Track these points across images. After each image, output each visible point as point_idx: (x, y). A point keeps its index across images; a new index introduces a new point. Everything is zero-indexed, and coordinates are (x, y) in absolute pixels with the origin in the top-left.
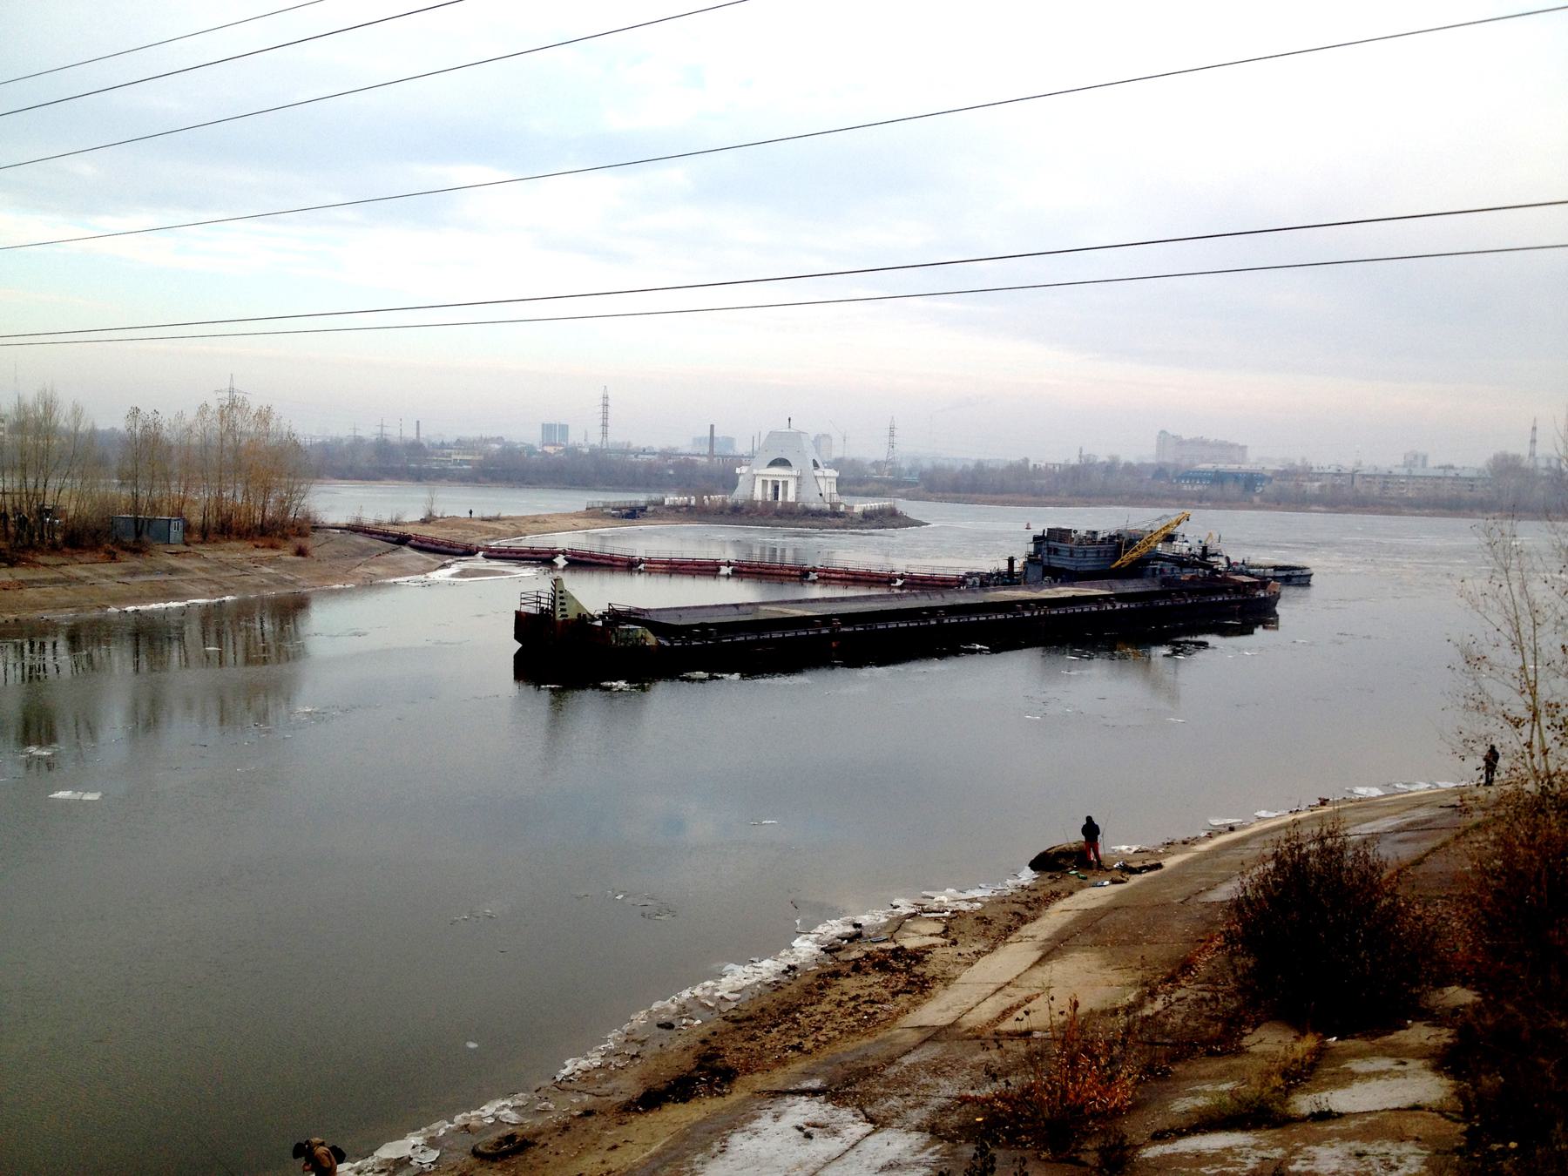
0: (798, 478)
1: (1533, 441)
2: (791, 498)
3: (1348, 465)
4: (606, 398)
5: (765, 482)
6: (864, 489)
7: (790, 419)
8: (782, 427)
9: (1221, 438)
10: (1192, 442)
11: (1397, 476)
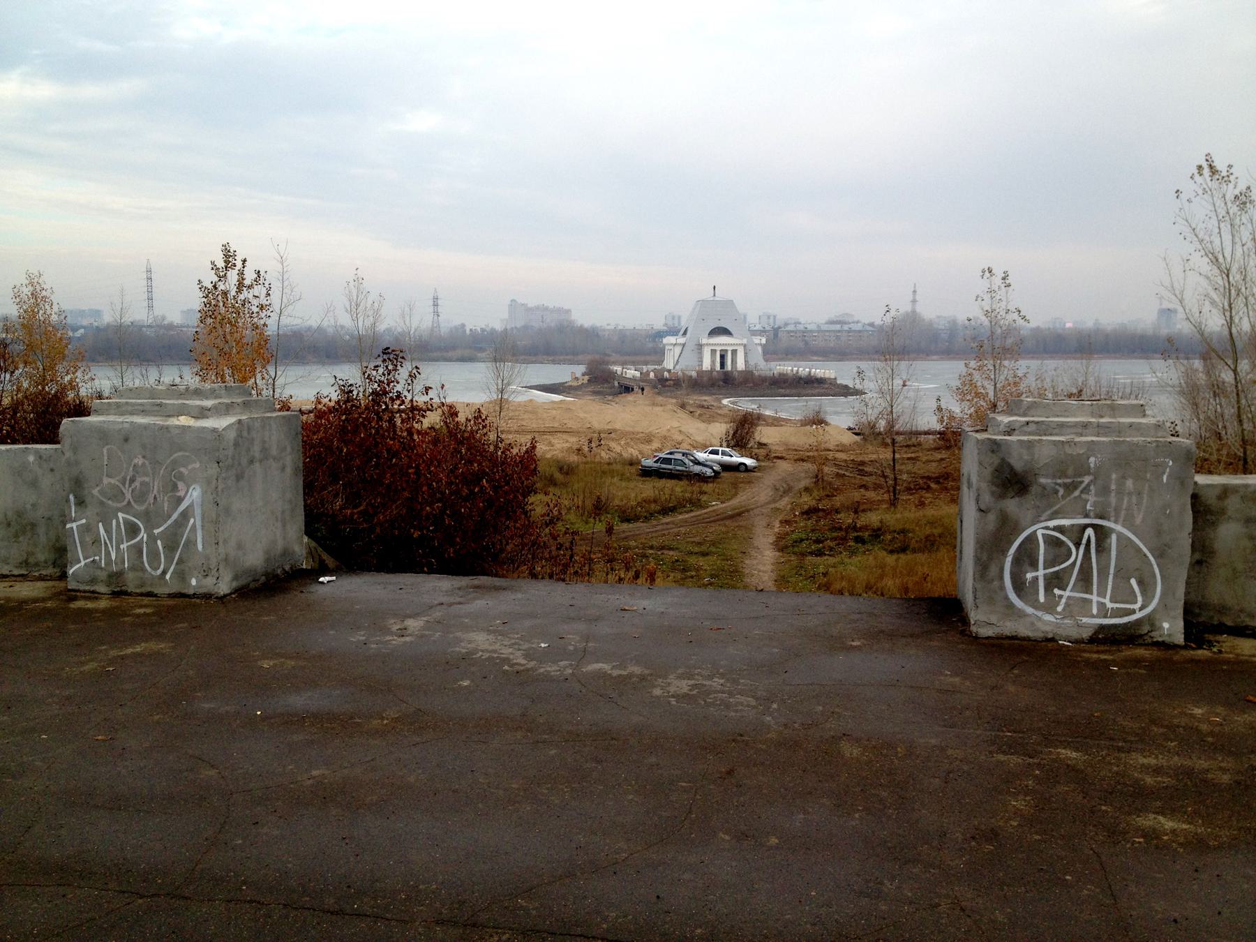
0: (745, 346)
1: (914, 301)
2: (741, 365)
3: (1089, 324)
4: (149, 271)
5: (713, 352)
6: (450, 354)
7: (714, 288)
8: (708, 295)
9: (557, 305)
10: (537, 308)
11: (811, 331)
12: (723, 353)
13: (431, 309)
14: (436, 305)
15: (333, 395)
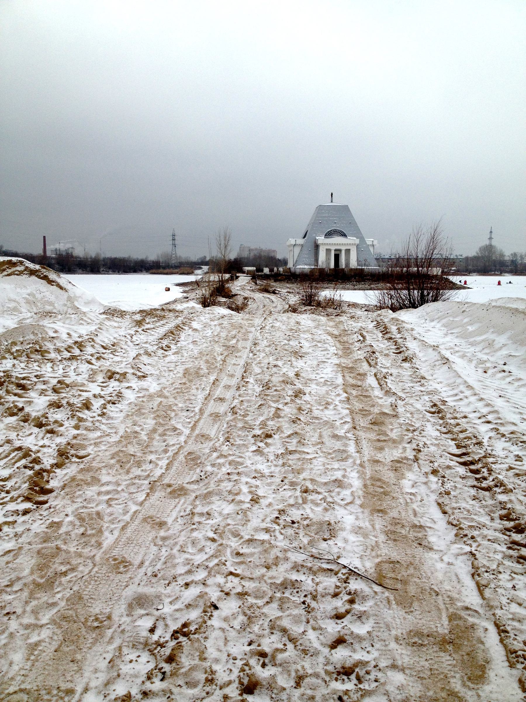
1: (491, 238)
5: (328, 251)
12: (337, 253)
13: (171, 242)
14: (174, 240)
15: (62, 275)
